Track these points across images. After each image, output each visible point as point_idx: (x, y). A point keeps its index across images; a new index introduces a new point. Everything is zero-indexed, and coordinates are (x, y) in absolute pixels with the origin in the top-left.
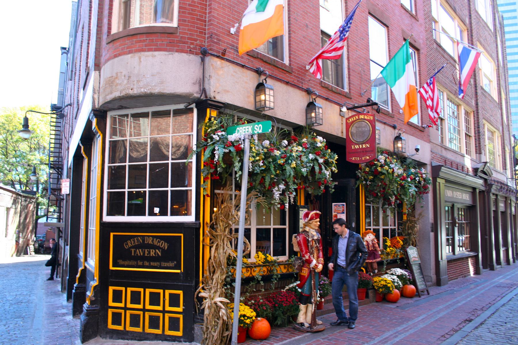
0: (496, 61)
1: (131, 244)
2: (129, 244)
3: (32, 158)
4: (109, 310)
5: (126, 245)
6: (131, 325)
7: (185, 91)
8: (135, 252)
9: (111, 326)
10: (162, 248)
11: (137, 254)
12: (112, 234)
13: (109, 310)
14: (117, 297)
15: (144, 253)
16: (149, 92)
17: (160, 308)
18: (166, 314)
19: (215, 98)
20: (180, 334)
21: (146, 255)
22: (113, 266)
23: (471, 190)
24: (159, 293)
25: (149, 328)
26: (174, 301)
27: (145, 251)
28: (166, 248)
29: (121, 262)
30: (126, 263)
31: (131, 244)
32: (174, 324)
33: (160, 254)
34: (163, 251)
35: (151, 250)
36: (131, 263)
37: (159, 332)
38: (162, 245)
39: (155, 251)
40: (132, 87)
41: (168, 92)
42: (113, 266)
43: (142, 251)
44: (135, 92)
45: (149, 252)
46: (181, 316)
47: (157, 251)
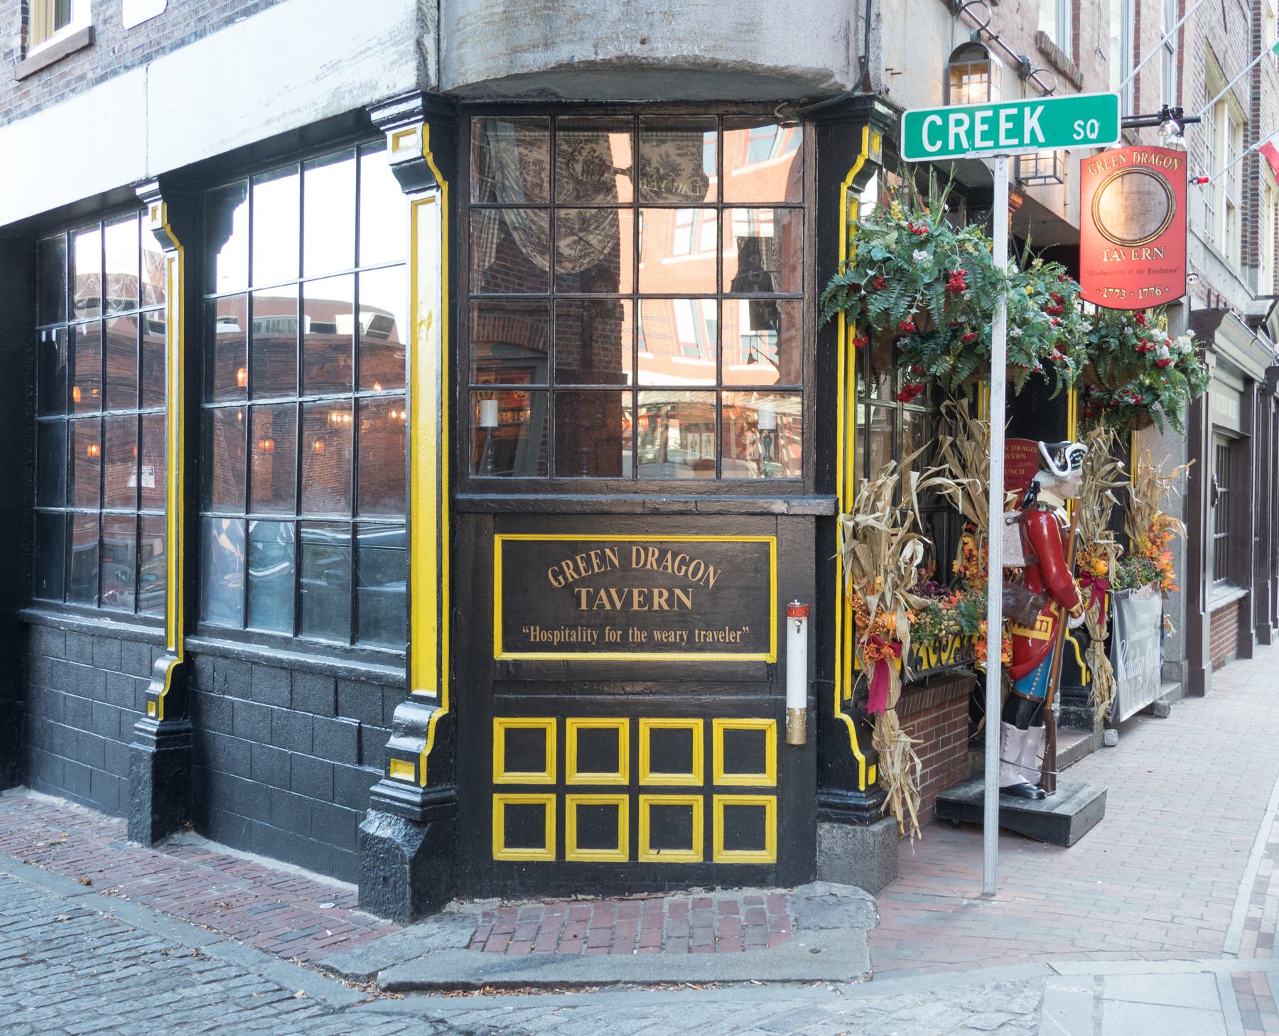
0: (1249, 15)
1: (577, 570)
2: (569, 572)
3: (1159, 334)
4: (496, 797)
5: (555, 575)
6: (657, 842)
7: (815, 66)
8: (591, 598)
9: (502, 852)
10: (695, 586)
11: (602, 606)
12: (498, 539)
13: (496, 797)
14: (526, 751)
15: (628, 602)
16: (708, 56)
17: (548, 777)
18: (716, 798)
19: (887, 91)
20: (767, 856)
21: (636, 607)
22: (507, 648)
23: (1239, 385)
24: (542, 732)
25: (579, 846)
26: (526, 751)
27: (630, 594)
28: (712, 582)
29: (536, 634)
30: (557, 637)
31: (577, 570)
32: (744, 828)
33: (688, 603)
34: (698, 589)
35: (656, 592)
36: (557, 637)
37: (693, 856)
38: (695, 574)
39: (671, 593)
40: (645, 33)
41: (769, 63)
42: (507, 648)
43: (620, 593)
44: (660, 54)
45: (648, 599)
46: (771, 803)
47: (678, 592)
